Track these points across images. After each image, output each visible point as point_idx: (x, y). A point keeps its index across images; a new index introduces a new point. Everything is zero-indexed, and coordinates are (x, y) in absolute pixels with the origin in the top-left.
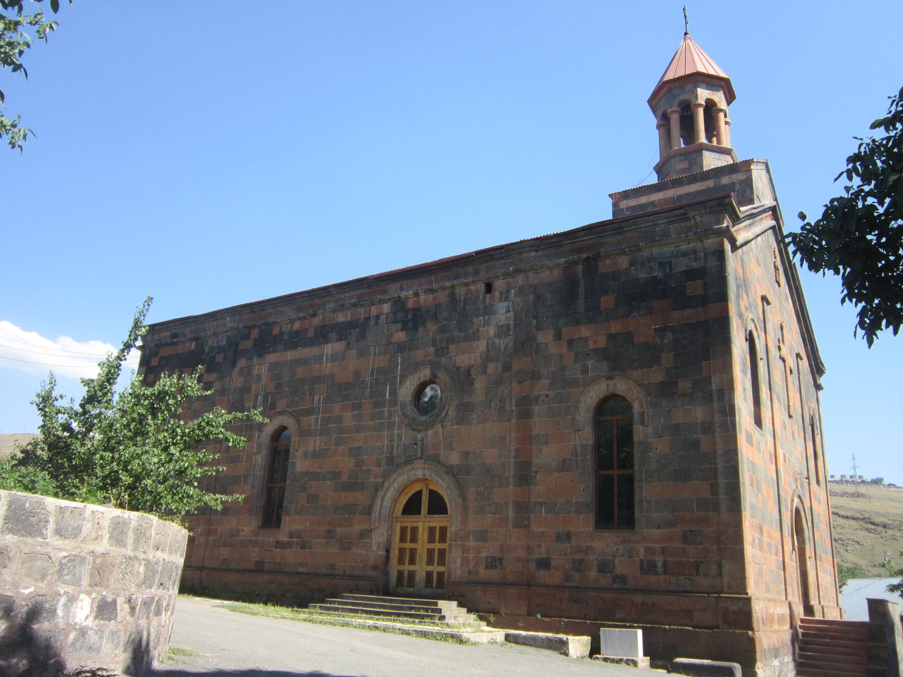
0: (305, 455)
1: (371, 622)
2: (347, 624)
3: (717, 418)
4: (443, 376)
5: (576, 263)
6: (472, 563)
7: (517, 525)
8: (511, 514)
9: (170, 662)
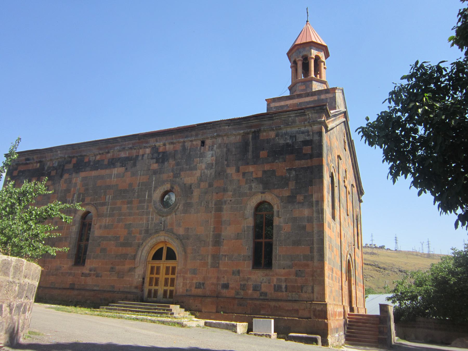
0: (100, 227)
1: (134, 316)
2: (122, 317)
3: (315, 215)
4: (177, 188)
5: (248, 133)
6: (188, 286)
7: (213, 266)
8: (210, 260)
9: (29, 339)
